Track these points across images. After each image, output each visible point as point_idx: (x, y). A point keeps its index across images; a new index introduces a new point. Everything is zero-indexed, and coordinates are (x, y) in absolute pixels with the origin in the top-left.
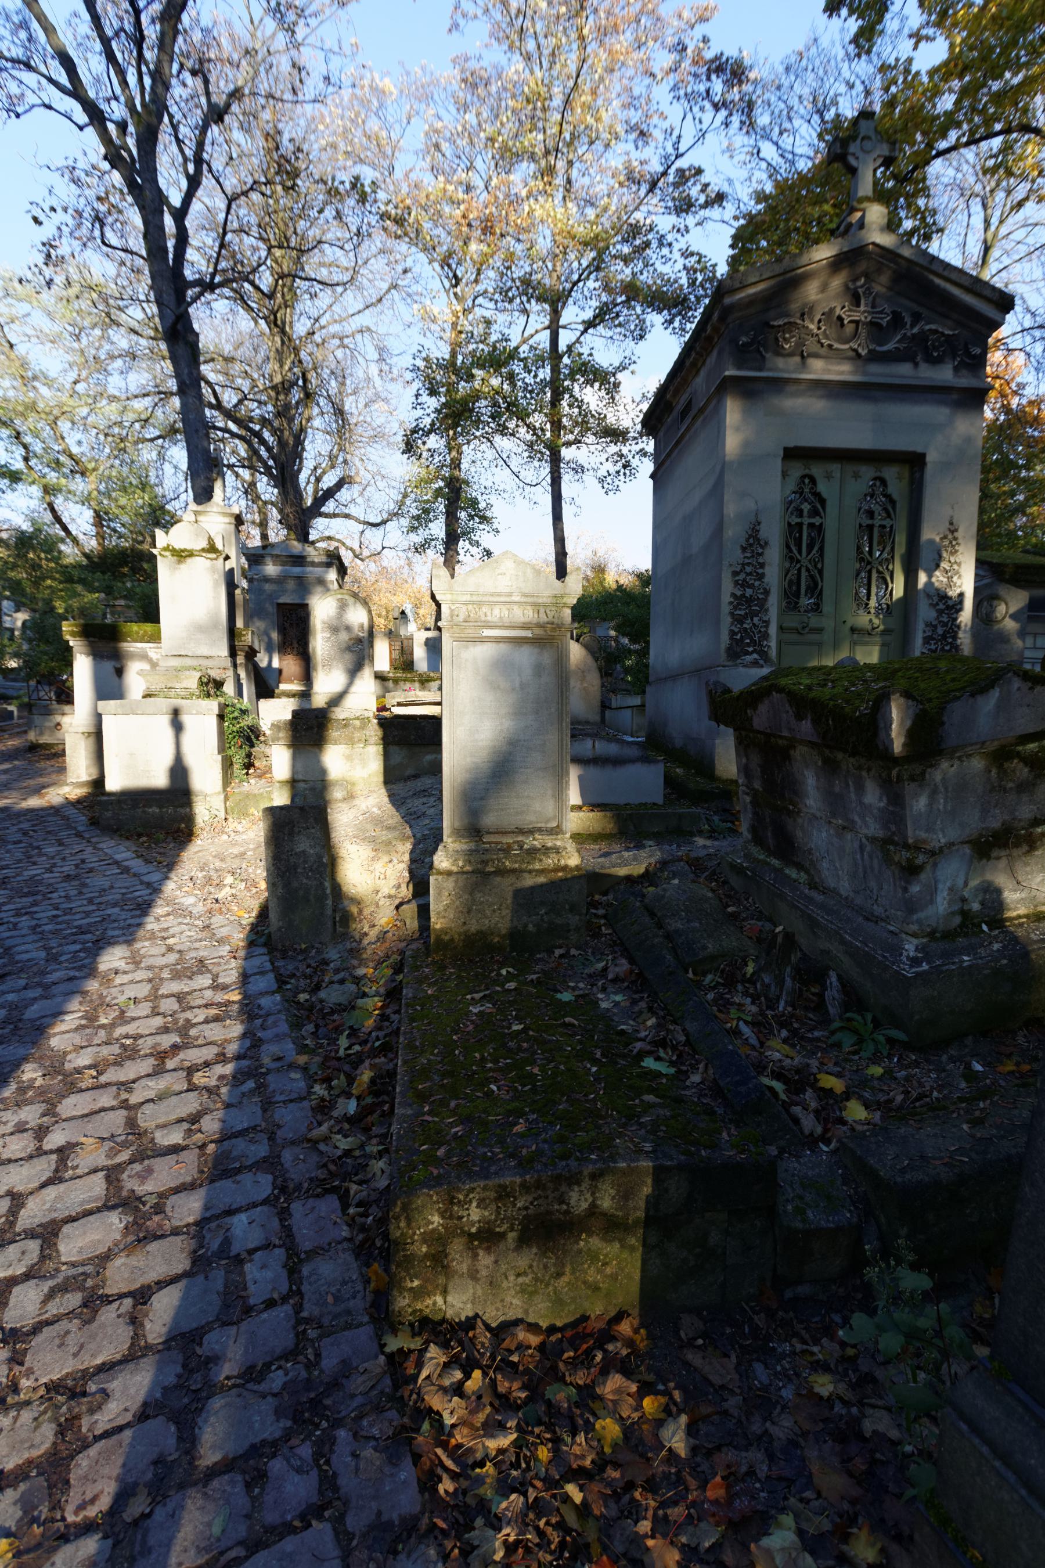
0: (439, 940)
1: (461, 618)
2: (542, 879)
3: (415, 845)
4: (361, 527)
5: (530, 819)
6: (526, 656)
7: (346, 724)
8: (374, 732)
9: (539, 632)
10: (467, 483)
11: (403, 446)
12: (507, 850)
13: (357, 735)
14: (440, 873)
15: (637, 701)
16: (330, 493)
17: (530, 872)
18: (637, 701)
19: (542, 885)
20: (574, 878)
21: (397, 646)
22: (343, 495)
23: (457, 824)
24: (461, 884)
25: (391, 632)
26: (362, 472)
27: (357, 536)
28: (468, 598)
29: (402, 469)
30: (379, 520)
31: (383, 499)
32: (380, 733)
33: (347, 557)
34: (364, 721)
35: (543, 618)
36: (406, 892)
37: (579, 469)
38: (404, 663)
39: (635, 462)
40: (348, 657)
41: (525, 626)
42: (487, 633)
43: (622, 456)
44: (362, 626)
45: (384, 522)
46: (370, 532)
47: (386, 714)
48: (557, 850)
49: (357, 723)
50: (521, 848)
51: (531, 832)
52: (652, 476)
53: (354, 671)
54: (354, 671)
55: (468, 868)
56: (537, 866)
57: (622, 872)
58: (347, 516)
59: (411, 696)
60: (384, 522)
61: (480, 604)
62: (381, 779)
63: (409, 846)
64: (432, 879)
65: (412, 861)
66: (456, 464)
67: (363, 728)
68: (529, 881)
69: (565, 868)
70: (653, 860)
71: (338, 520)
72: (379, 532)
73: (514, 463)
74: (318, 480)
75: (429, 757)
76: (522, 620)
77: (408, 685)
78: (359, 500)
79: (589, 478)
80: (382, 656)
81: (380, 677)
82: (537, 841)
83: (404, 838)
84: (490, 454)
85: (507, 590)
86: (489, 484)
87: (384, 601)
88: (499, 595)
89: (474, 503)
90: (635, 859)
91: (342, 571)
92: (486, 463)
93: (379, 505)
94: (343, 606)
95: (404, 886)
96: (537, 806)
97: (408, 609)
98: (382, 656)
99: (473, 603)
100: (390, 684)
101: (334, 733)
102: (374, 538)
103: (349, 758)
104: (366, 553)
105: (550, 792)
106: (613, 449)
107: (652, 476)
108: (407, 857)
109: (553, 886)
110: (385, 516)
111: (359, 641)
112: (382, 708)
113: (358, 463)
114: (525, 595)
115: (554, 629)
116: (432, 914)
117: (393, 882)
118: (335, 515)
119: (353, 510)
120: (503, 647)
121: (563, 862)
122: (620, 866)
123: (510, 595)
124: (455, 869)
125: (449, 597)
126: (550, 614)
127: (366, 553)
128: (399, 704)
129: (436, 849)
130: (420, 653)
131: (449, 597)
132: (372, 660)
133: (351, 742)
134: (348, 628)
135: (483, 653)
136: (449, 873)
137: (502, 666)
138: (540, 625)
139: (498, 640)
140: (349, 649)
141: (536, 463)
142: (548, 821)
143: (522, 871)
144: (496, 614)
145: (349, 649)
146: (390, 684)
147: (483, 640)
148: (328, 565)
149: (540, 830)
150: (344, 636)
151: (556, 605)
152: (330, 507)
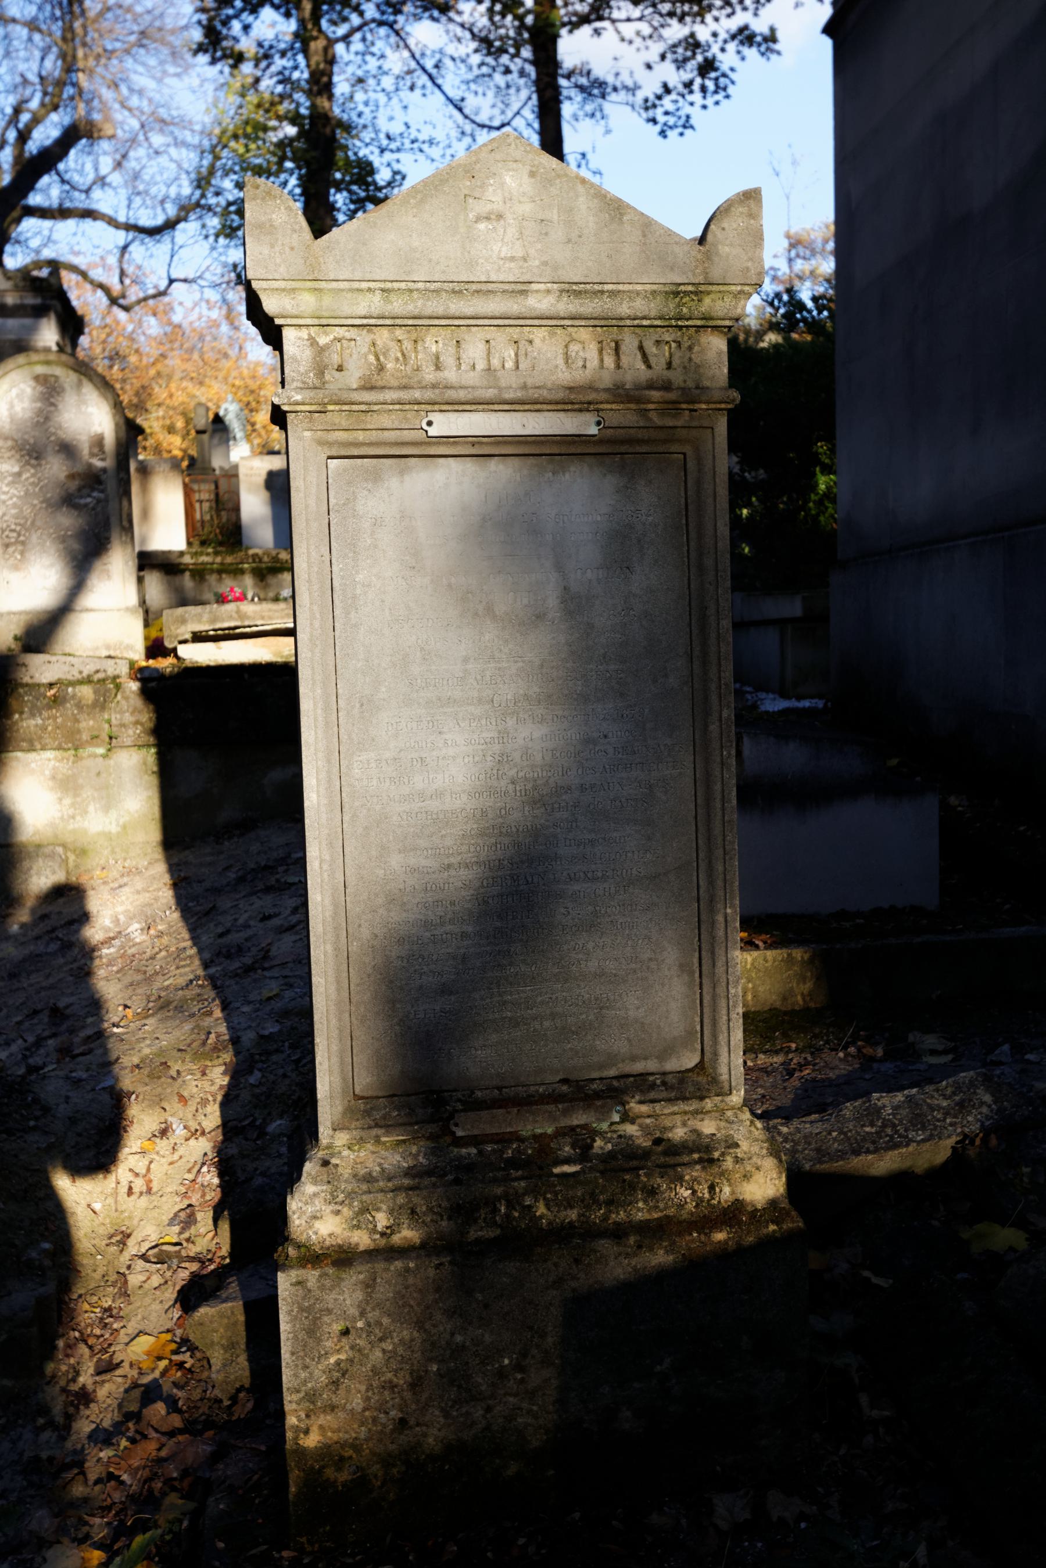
0: (314, 1480)
1: (353, 376)
2: (660, 1257)
3: (237, 1074)
4: (121, 237)
5: (615, 1050)
6: (582, 500)
7: (57, 696)
8: (130, 713)
9: (621, 416)
10: (348, 128)
11: (197, 35)
12: (537, 1162)
13: (87, 724)
14: (313, 1258)
15: (792, 607)
16: (49, 159)
17: (618, 1233)
18: (792, 607)
19: (661, 1275)
20: (767, 1243)
21: (204, 492)
22: (76, 163)
23: (364, 1082)
24: (384, 1291)
25: (193, 461)
26: (119, 115)
27: (112, 260)
28: (371, 304)
29: (197, 95)
30: (159, 221)
31: (168, 171)
32: (146, 717)
33: (83, 299)
34: (105, 687)
35: (635, 370)
36: (211, 1239)
37: (595, 89)
38: (218, 526)
39: (727, 60)
40: (68, 521)
41: (571, 400)
42: (444, 424)
43: (697, 45)
44: (98, 442)
45: (170, 225)
46: (138, 251)
47: (165, 664)
48: (705, 1153)
49: (86, 692)
50: (584, 1151)
51: (614, 1092)
52: (828, 30)
53: (85, 555)
54: (85, 555)
55: (408, 1234)
56: (641, 1212)
57: (884, 1164)
58: (89, 214)
59: (227, 616)
60: (170, 225)
61: (417, 324)
62: (153, 834)
63: (218, 1078)
64: (284, 1281)
65: (229, 1128)
66: (321, 83)
67: (101, 704)
68: (618, 1265)
69: (735, 1213)
70: (972, 1123)
71: (71, 223)
72: (161, 248)
73: (452, 80)
74: (23, 137)
75: (277, 775)
76: (564, 376)
77: (227, 584)
78: (115, 178)
79: (615, 107)
80: (165, 520)
81: (148, 562)
82: (635, 1124)
83: (201, 1052)
84: (396, 61)
85: (510, 273)
86: (396, 128)
87: (180, 398)
88: (483, 289)
89: (365, 170)
90: (918, 1121)
91: (72, 325)
92: (388, 82)
93: (159, 190)
94: (50, 392)
95: (205, 1218)
96: (631, 1005)
97: (230, 410)
98: (165, 520)
99: (393, 322)
100: (187, 581)
101: (27, 723)
102: (151, 261)
103: (66, 785)
104: (134, 294)
105: (671, 955)
106: (676, 31)
107: (828, 30)
108: (212, 1118)
109: (697, 1270)
110: (172, 211)
111: (92, 479)
112: (156, 648)
113: (107, 94)
114: (572, 290)
115: (671, 408)
116: (291, 1402)
117: (172, 1205)
118: (62, 213)
119: (103, 201)
120: (502, 473)
121: (726, 1193)
122: (876, 1146)
123: (521, 289)
124: (362, 1239)
125: (307, 302)
126: (659, 356)
127: (134, 294)
128: (198, 638)
129: (292, 1177)
130: (254, 505)
131: (307, 302)
132: (128, 528)
133: (72, 742)
134: (67, 449)
135: (441, 492)
136: (342, 1258)
137: (507, 534)
138: (620, 394)
139: (483, 449)
140: (68, 501)
141: (499, 79)
142: (667, 1051)
143: (590, 1233)
144: (476, 358)
145: (68, 501)
146: (187, 581)
147: (430, 450)
148: (39, 312)
149: (643, 1084)
150: (56, 468)
151: (676, 323)
152: (47, 191)
